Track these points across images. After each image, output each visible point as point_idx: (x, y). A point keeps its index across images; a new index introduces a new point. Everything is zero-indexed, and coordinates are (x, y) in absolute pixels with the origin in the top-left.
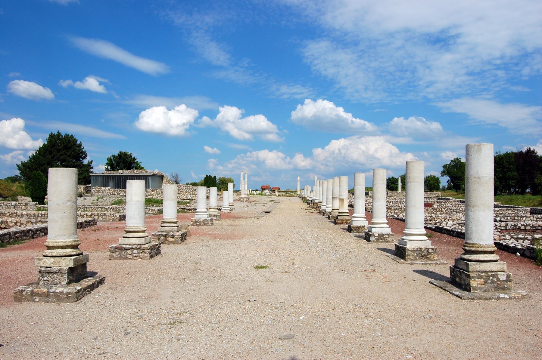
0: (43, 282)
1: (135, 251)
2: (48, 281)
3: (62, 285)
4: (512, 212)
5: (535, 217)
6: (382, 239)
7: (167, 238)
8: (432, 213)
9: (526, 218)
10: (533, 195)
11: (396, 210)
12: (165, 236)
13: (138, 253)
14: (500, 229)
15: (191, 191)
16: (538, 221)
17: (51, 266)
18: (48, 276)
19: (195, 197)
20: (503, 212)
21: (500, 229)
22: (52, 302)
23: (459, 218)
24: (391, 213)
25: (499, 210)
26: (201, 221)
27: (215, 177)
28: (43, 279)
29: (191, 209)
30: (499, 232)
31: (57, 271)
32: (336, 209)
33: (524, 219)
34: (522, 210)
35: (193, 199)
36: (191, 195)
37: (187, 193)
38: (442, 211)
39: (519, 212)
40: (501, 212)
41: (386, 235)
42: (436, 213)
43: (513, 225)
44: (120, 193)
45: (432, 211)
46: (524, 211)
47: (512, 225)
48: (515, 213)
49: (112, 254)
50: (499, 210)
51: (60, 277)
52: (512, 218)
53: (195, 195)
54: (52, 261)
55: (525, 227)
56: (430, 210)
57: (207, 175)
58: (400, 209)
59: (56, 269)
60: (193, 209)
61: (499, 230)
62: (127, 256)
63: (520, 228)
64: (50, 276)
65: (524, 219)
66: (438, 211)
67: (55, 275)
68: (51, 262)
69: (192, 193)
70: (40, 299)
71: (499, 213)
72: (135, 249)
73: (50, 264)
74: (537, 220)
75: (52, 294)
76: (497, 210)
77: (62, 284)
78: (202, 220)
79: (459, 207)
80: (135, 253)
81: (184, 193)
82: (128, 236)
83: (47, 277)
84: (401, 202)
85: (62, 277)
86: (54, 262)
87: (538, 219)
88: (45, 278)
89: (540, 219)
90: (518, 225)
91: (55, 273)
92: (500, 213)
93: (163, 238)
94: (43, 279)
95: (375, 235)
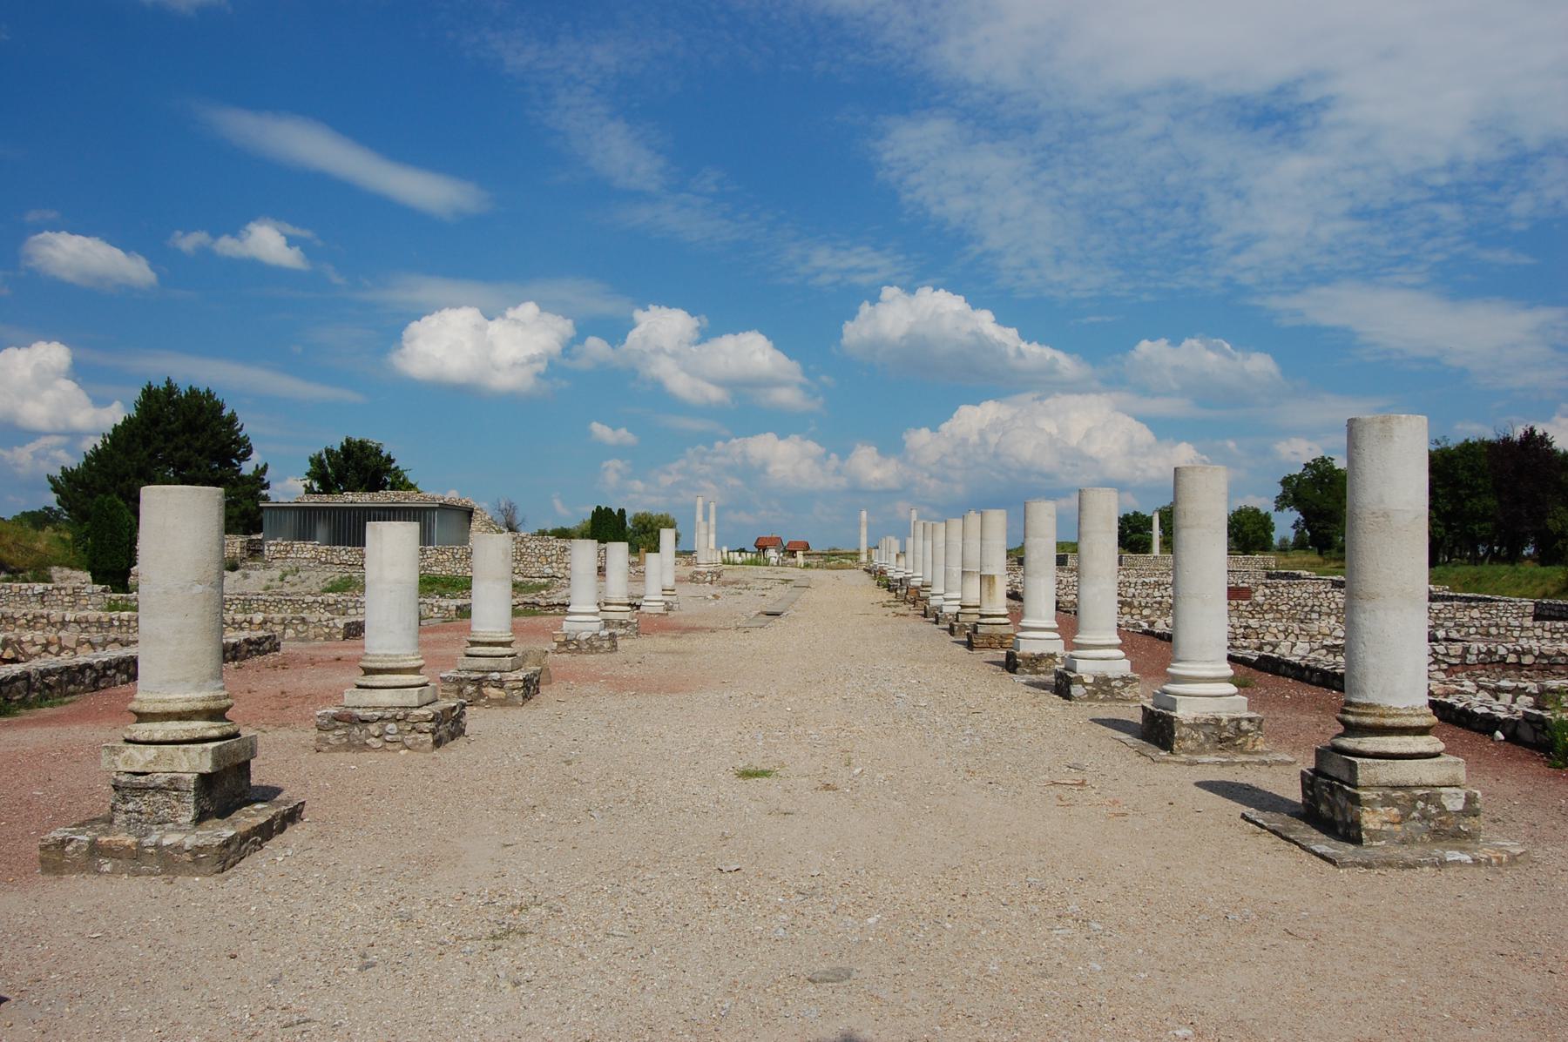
0: (123, 817)
1: (391, 726)
2: (140, 813)
3: (180, 825)
4: (1481, 613)
5: (1547, 629)
6: (1104, 692)
8: (1250, 616)
9: (1521, 631)
11: (1146, 607)
12: (478, 683)
13: (400, 732)
14: (1445, 662)
15: (554, 552)
16: (1558, 639)
18: (138, 799)
19: (563, 571)
20: (1454, 614)
21: (1445, 662)
22: (151, 873)
23: (1328, 632)
24: (1132, 615)
25: (1443, 607)
26: (583, 638)
27: (622, 512)
28: (124, 807)
29: (554, 605)
30: (1445, 671)
31: (166, 786)
33: (1516, 634)
34: (1510, 608)
35: (559, 575)
36: (554, 564)
37: (543, 559)
38: (1277, 611)
39: (1501, 614)
40: (1450, 613)
41: (1115, 679)
42: (1261, 616)
43: (1484, 650)
44: (346, 557)
45: (1250, 612)
46: (1515, 611)
47: (1480, 652)
48: (1489, 616)
50: (1443, 607)
51: (173, 802)
52: (1481, 631)
53: (563, 565)
54: (150, 755)
55: (1519, 658)
56: (1244, 607)
57: (599, 508)
58: (1156, 606)
59: (161, 780)
60: (558, 604)
61: (1444, 666)
62: (368, 741)
63: (1506, 659)
64: (146, 798)
65: (1516, 634)
66: (1266, 612)
67: (159, 797)
68: (149, 758)
69: (554, 558)
71: (1442, 615)
72: (392, 722)
73: (146, 765)
74: (1554, 636)
75: (150, 851)
76: (1438, 608)
77: (180, 822)
78: (584, 636)
79: (1329, 599)
80: (390, 732)
81: (533, 560)
82: (369, 684)
83: (138, 803)
84: (1159, 585)
85: (178, 801)
86: (157, 758)
87: (1555, 633)
88: (131, 806)
89: (1562, 633)
91: (159, 789)
92: (1448, 615)
93: (470, 689)
94: (124, 807)
95: (1085, 681)
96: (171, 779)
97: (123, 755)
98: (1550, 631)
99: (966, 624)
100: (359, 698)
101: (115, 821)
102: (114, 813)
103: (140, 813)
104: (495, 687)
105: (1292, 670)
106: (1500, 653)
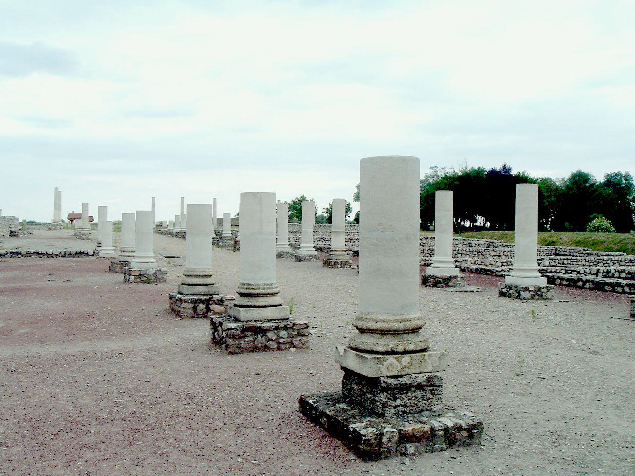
0: (393, 411)
2: (405, 406)
6: (538, 295)
7: (210, 306)
10: (617, 232)
12: (207, 303)
17: (403, 373)
18: (404, 396)
22: (442, 450)
23: (494, 264)
28: (394, 404)
29: (31, 253)
31: (425, 383)
32: (340, 250)
41: (544, 288)
43: (605, 271)
46: (547, 252)
47: (604, 272)
49: (237, 342)
51: (428, 395)
55: (619, 274)
59: (421, 379)
60: (34, 253)
64: (409, 394)
70: (417, 449)
73: (402, 369)
77: (435, 409)
78: (151, 271)
80: (283, 336)
82: (257, 304)
85: (432, 394)
87: (590, 262)
88: (399, 402)
90: (612, 272)
91: (420, 387)
94: (394, 404)
95: (530, 289)
96: (429, 378)
97: (386, 364)
98: (588, 262)
99: (338, 261)
100: (252, 315)
101: (386, 415)
102: (385, 409)
103: (405, 406)
104: (217, 305)
105: (566, 282)
106: (612, 272)
